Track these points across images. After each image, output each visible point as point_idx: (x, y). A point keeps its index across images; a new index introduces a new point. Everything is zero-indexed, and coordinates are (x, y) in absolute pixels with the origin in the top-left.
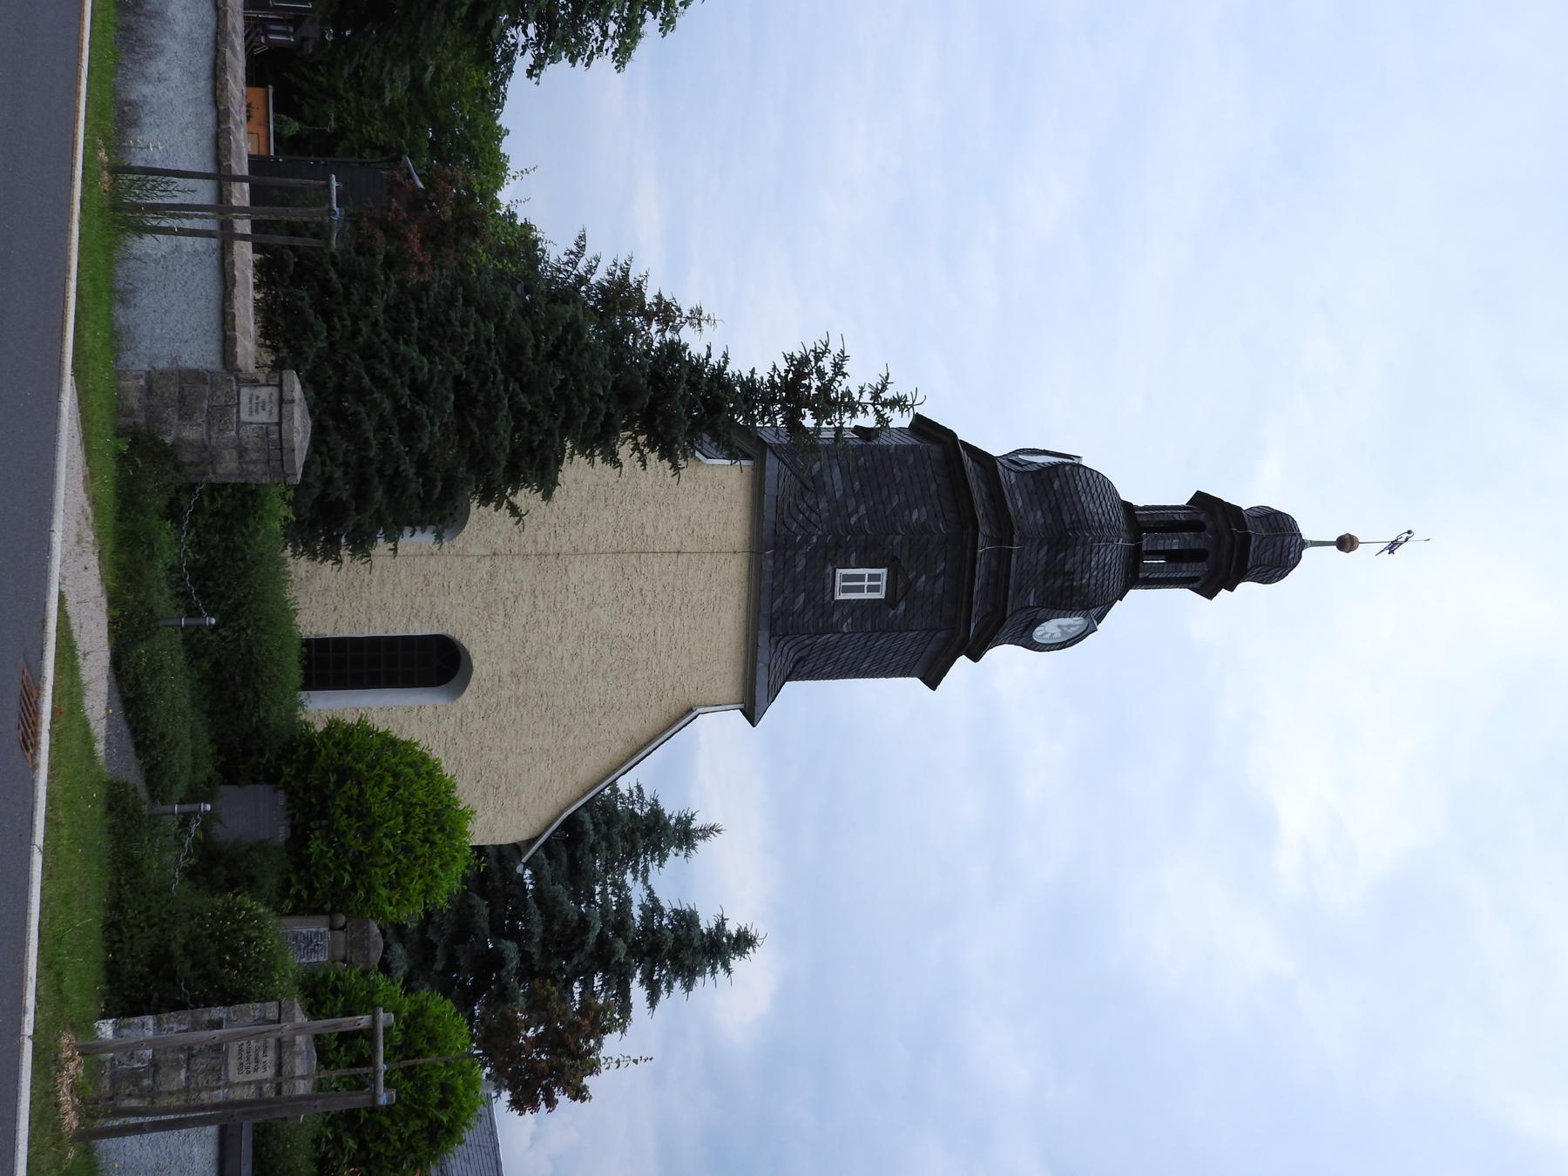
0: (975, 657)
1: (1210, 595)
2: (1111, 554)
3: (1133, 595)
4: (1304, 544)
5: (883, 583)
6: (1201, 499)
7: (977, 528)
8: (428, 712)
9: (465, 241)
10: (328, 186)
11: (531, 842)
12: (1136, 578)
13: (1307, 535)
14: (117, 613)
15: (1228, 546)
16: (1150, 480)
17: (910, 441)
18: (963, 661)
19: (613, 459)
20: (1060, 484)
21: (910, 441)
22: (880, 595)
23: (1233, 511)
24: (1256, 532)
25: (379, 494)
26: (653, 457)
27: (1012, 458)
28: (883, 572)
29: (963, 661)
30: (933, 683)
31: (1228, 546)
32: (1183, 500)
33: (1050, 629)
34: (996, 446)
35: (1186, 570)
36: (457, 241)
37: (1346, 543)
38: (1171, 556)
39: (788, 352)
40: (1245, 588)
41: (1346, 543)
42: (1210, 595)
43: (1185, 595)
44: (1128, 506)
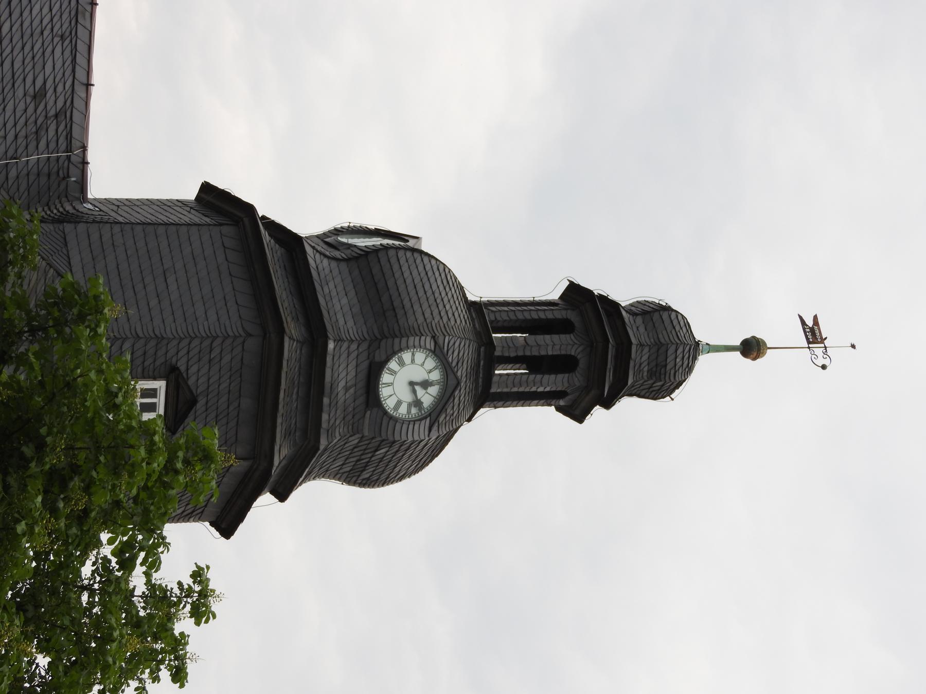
0: (282, 496)
1: (580, 418)
3: (486, 415)
4: (695, 349)
6: (575, 293)
7: (281, 332)
9: (86, 582)
10: (500, 375)
13: (700, 333)
15: (599, 351)
16: (500, 264)
17: (196, 218)
18: (266, 500)
20: (384, 277)
21: (196, 218)
24: (636, 332)
26: (169, 588)
27: (331, 240)
28: (160, 385)
29: (266, 500)
31: (599, 351)
32: (555, 296)
34: (306, 222)
35: (550, 382)
36: (60, 333)
37: (752, 348)
38: (537, 364)
40: (628, 405)
41: (752, 348)
42: (580, 418)
43: (546, 416)
44: (477, 308)
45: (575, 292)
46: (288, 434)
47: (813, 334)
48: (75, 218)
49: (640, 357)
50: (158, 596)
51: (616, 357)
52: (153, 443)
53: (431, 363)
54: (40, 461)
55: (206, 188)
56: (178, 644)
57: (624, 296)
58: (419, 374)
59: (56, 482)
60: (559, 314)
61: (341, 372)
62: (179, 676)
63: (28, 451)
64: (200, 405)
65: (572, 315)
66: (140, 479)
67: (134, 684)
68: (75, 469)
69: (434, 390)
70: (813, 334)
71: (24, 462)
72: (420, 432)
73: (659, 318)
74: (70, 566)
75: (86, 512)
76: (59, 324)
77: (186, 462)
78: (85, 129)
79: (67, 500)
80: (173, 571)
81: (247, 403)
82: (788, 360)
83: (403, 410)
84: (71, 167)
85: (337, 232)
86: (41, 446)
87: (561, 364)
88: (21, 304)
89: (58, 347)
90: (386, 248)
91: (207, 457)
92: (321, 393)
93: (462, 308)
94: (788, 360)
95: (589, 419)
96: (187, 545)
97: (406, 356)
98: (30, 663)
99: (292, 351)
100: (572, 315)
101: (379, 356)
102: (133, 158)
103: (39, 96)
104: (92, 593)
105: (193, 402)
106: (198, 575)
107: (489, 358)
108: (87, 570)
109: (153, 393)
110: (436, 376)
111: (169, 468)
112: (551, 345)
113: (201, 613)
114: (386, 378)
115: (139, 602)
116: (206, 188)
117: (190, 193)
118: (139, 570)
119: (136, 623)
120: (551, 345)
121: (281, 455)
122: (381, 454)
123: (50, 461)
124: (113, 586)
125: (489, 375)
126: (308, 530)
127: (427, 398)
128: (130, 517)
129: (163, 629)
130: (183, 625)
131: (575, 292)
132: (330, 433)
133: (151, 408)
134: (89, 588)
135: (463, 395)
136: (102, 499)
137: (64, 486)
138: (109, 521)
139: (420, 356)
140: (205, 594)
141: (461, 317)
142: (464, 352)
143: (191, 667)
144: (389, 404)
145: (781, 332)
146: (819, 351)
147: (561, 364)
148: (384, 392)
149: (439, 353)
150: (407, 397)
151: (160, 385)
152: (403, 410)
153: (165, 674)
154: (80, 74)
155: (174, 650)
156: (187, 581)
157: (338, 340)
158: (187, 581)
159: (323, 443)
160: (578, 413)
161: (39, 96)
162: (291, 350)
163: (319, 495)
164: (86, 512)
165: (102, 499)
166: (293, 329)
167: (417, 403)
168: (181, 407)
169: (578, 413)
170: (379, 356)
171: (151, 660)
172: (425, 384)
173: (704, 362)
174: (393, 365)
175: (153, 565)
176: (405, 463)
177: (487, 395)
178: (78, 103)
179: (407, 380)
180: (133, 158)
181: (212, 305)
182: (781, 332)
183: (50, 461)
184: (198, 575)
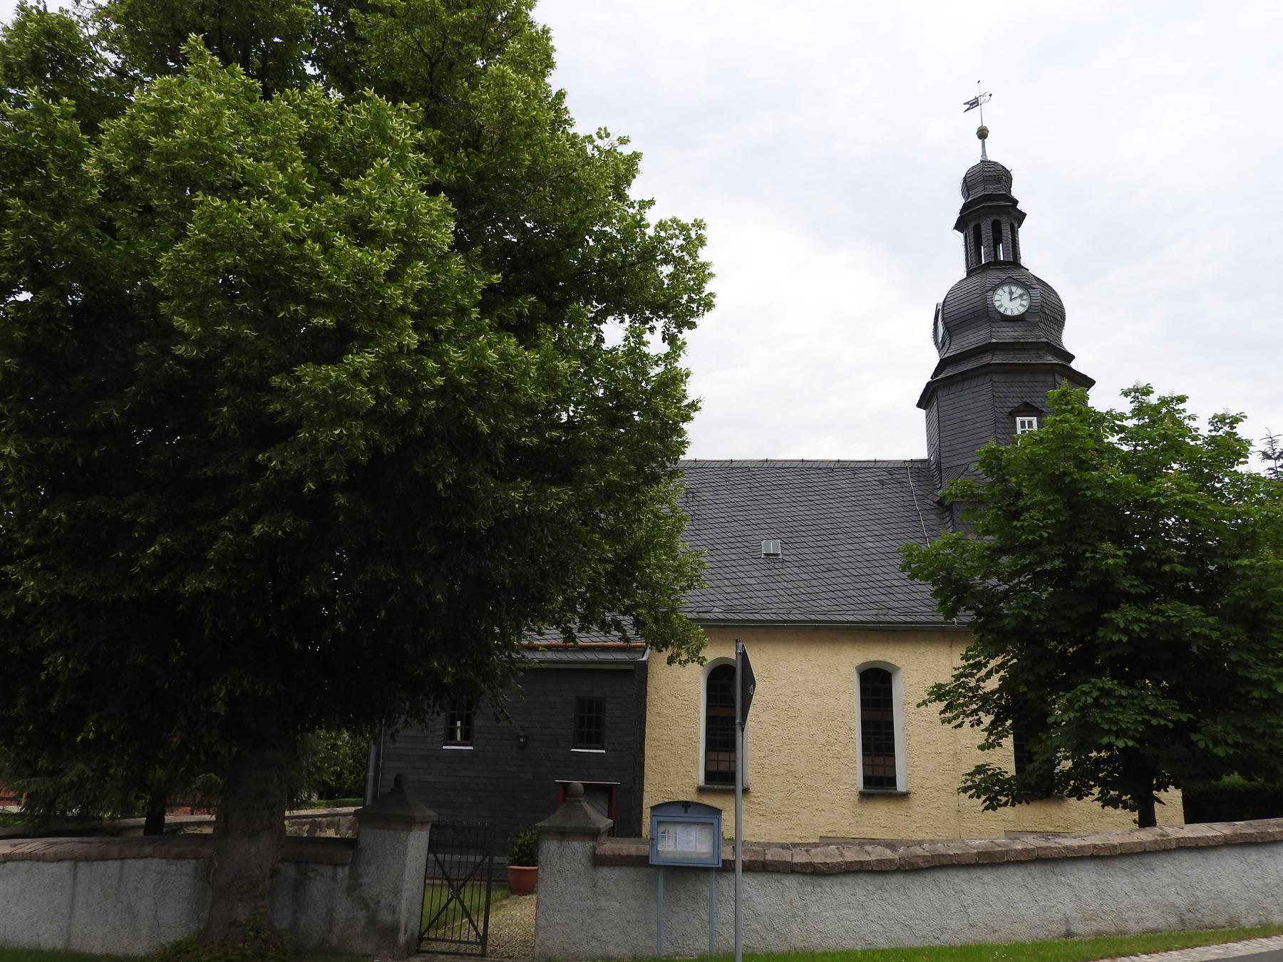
0: (1072, 357)
3: (1024, 261)
5: (1026, 419)
7: (989, 365)
8: (763, 717)
15: (989, 210)
16: (947, 263)
18: (1073, 365)
20: (955, 319)
22: (1034, 420)
23: (966, 207)
24: (978, 193)
25: (1239, 738)
27: (940, 346)
28: (1019, 420)
29: (1073, 365)
31: (989, 210)
32: (961, 235)
34: (932, 358)
35: (1006, 232)
37: (982, 134)
38: (997, 240)
39: (855, 797)
40: (1015, 192)
41: (982, 134)
43: (1023, 232)
44: (970, 273)
45: (960, 226)
46: (1040, 357)
47: (974, 103)
48: (939, 464)
49: (991, 189)
50: (1138, 413)
51: (991, 201)
52: (1061, 421)
53: (1000, 292)
54: (1073, 473)
55: (919, 405)
56: (1164, 401)
57: (960, 202)
58: (1007, 296)
59: (1082, 465)
60: (971, 232)
61: (1007, 334)
62: (1182, 399)
63: (1068, 480)
64: (1028, 400)
65: (971, 226)
66: (1079, 426)
67: (1186, 422)
68: (1076, 457)
69: (1014, 289)
70: (974, 103)
71: (1073, 481)
72: (1036, 293)
73: (969, 184)
74: (1125, 457)
75: (1097, 450)
76: (1000, 468)
77: (1067, 404)
78: (896, 462)
79: (1092, 460)
80: (1126, 406)
81: (1025, 378)
82: (988, 115)
83: (1025, 303)
84: (915, 468)
85: (936, 343)
86: (1065, 474)
87: (996, 228)
88: (991, 485)
89: (1011, 468)
90: (943, 319)
91: (1064, 394)
92: (1019, 343)
93: (970, 280)
94: (988, 115)
96: (1102, 399)
97: (997, 304)
98: (461, 416)
99: (998, 359)
100: (971, 226)
101: (998, 317)
102: (909, 440)
103: (882, 483)
104: (1137, 445)
105: (1026, 403)
106: (1126, 394)
107: (995, 264)
108: (1125, 448)
109: (1023, 424)
110: (1006, 289)
111: (1071, 411)
112: (987, 234)
113: (1147, 391)
114: (1008, 313)
115: (1142, 422)
116: (919, 405)
117: (923, 412)
118: (1126, 423)
119: (1153, 422)
120: (987, 234)
121: (1051, 360)
122: (1048, 311)
123: (1072, 469)
124: (1131, 435)
125: (1004, 263)
126: (1083, 342)
127: (1018, 291)
128: (1097, 430)
129: (1156, 409)
130: (1153, 400)
131: (960, 226)
132: (1040, 337)
133: (1030, 423)
134: (1135, 446)
135: (1015, 274)
136: (1091, 443)
137: (1085, 462)
138: (1099, 440)
139: (997, 297)
140: (1136, 390)
141: (976, 280)
142: (993, 277)
143: (1177, 394)
144: (1022, 310)
146: (982, 99)
147: (996, 228)
148: (1016, 313)
149: (994, 289)
150: (1018, 301)
151: (1019, 420)
152: (1025, 303)
153: (1181, 406)
154: (871, 465)
155: (1168, 403)
156: (1129, 399)
157: (991, 337)
158: (1129, 399)
159: (1044, 340)
160: (1022, 216)
161: (882, 483)
162: (998, 359)
163: (1070, 340)
164: (1097, 450)
165: (1091, 443)
166: (987, 359)
167: (1021, 296)
168: (1028, 409)
169: (1022, 216)
170: (998, 317)
171: (1172, 413)
172: (1011, 293)
173: (991, 157)
174: (1002, 310)
175: (1122, 417)
176: (1052, 299)
177: (1015, 262)
178: (884, 465)
179: (1009, 302)
180: (909, 440)
181: (976, 400)
182: (973, 120)
183: (1072, 469)
184: (1126, 394)
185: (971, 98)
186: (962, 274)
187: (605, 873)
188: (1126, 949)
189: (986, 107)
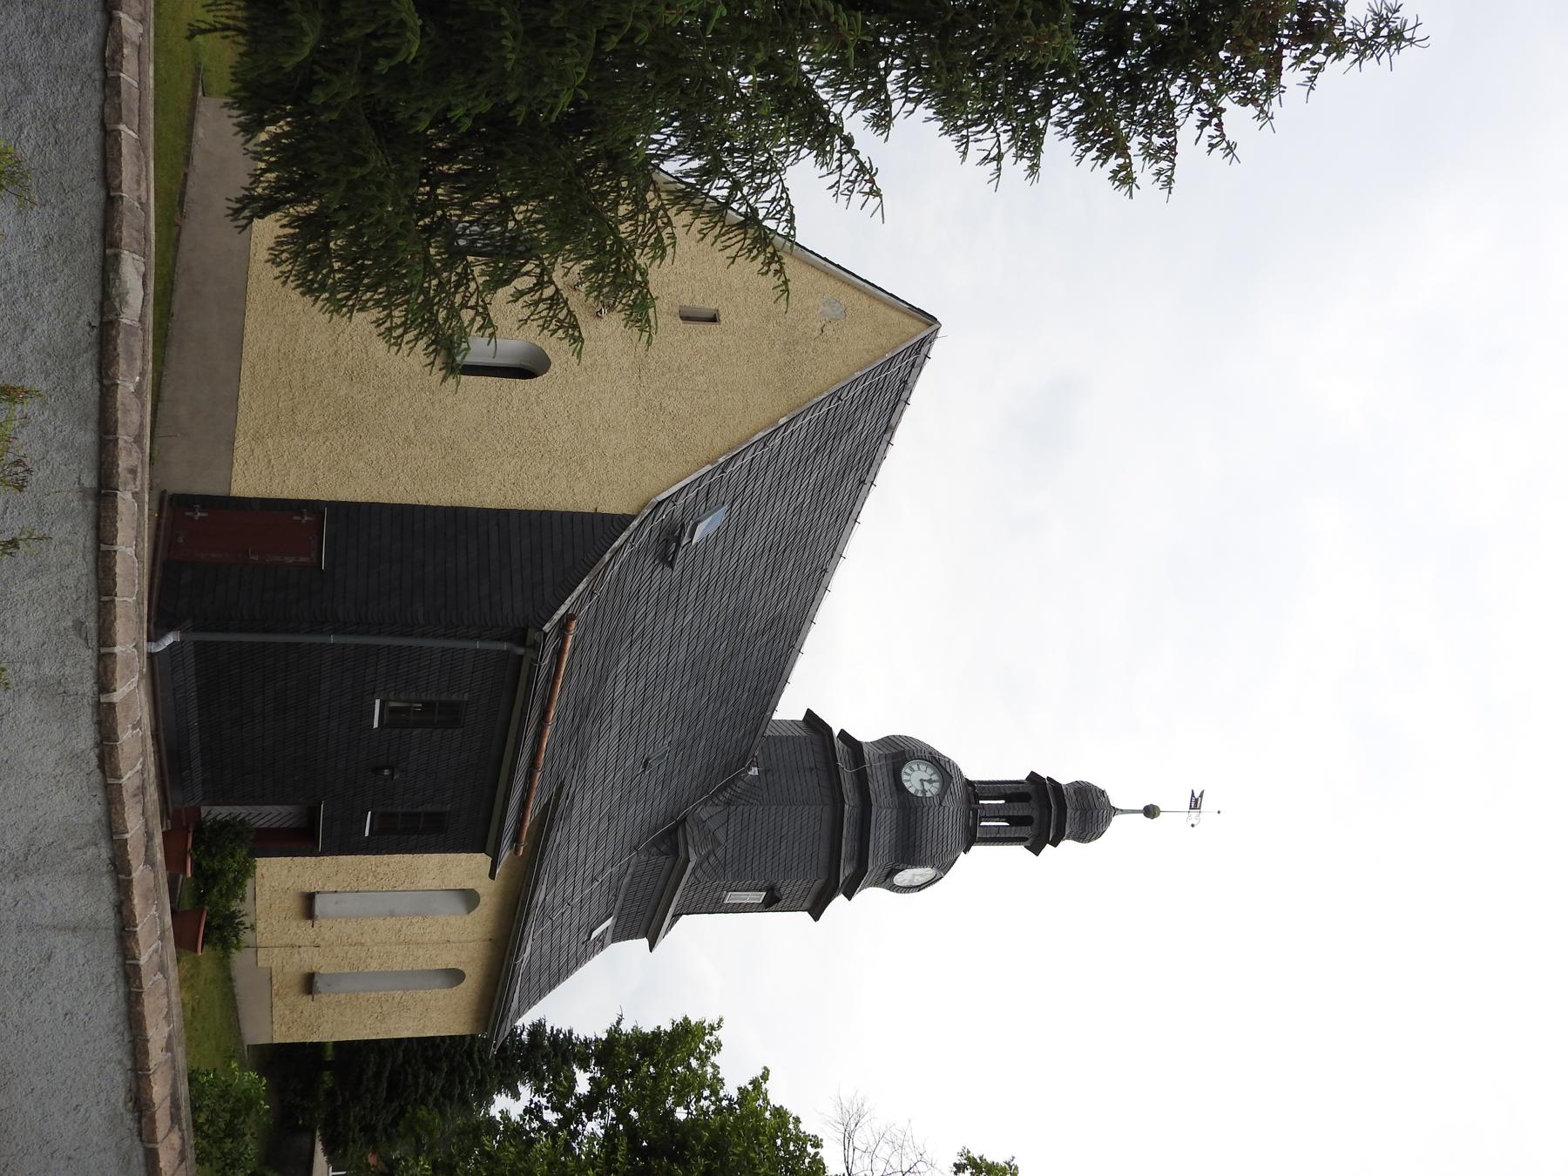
0: (849, 897)
2: (951, 815)
8: (473, 494)
11: (676, 917)
12: (971, 839)
13: (1115, 802)
14: (329, 1055)
15: (1049, 812)
16: (988, 759)
19: (1030, 143)
23: (1056, 786)
29: (840, 899)
30: (816, 918)
31: (1049, 812)
32: (1023, 776)
33: (904, 877)
35: (1025, 831)
37: (1151, 811)
40: (1067, 845)
41: (1151, 811)
43: (1019, 851)
44: (970, 783)
45: (1033, 777)
57: (1064, 779)
69: (937, 785)
95: (856, 897)
112: (1019, 810)
117: (800, 716)
120: (1019, 810)
121: (846, 871)
125: (975, 825)
144: (912, 791)
145: (1173, 801)
154: (904, 396)
160: (1036, 849)
162: (848, 785)
172: (930, 781)
182: (1173, 801)
185: (1206, 804)
186: (972, 775)
187: (317, 912)
188: (175, 230)
189: (1183, 820)
